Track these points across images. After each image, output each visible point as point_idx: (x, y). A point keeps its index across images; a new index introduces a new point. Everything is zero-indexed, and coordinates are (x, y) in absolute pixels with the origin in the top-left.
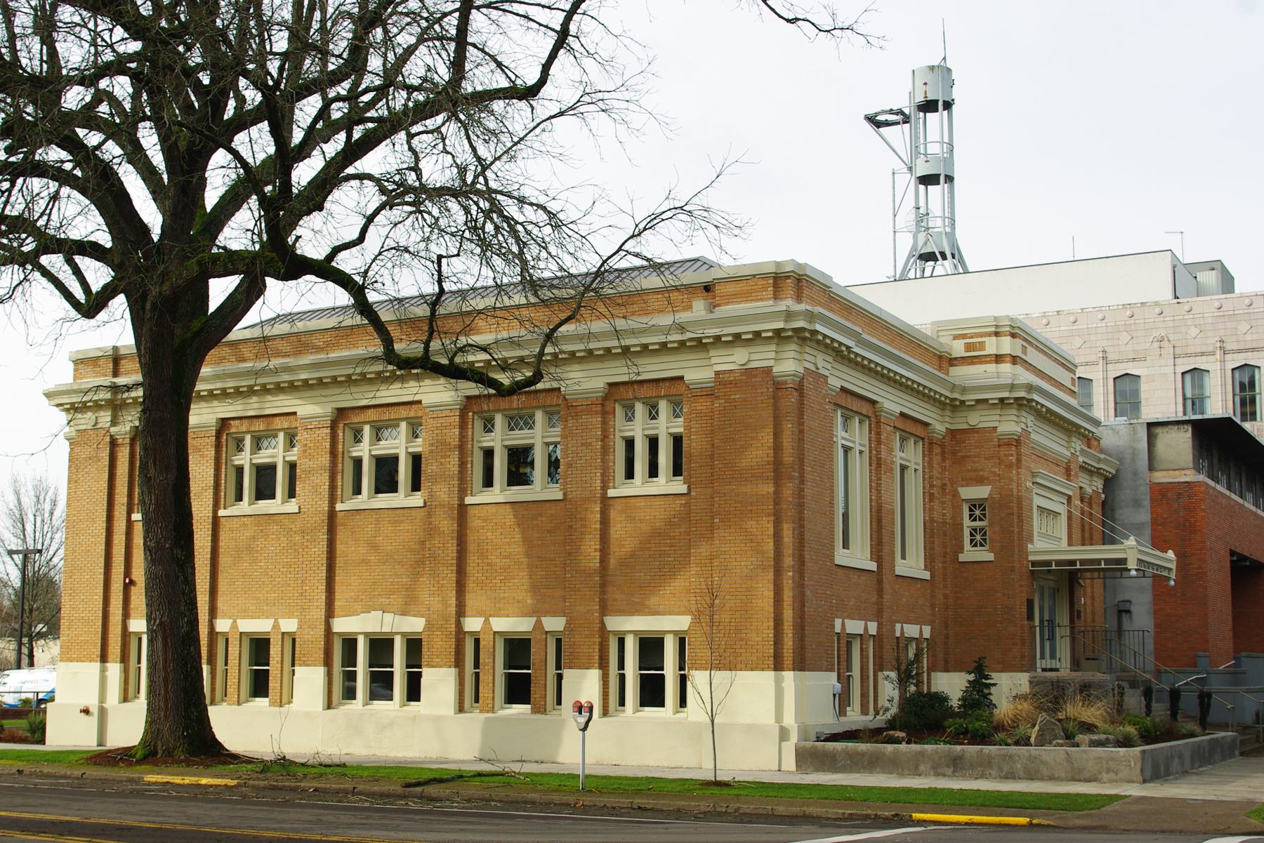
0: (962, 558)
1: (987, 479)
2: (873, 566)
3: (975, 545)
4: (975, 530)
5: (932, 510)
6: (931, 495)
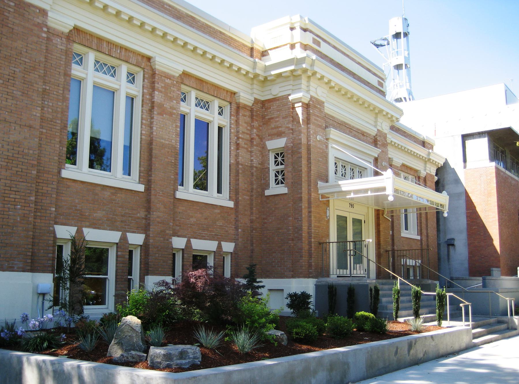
0: (267, 193)
1: (284, 133)
2: (141, 188)
3: (278, 184)
4: (278, 172)
5: (237, 156)
6: (238, 145)
